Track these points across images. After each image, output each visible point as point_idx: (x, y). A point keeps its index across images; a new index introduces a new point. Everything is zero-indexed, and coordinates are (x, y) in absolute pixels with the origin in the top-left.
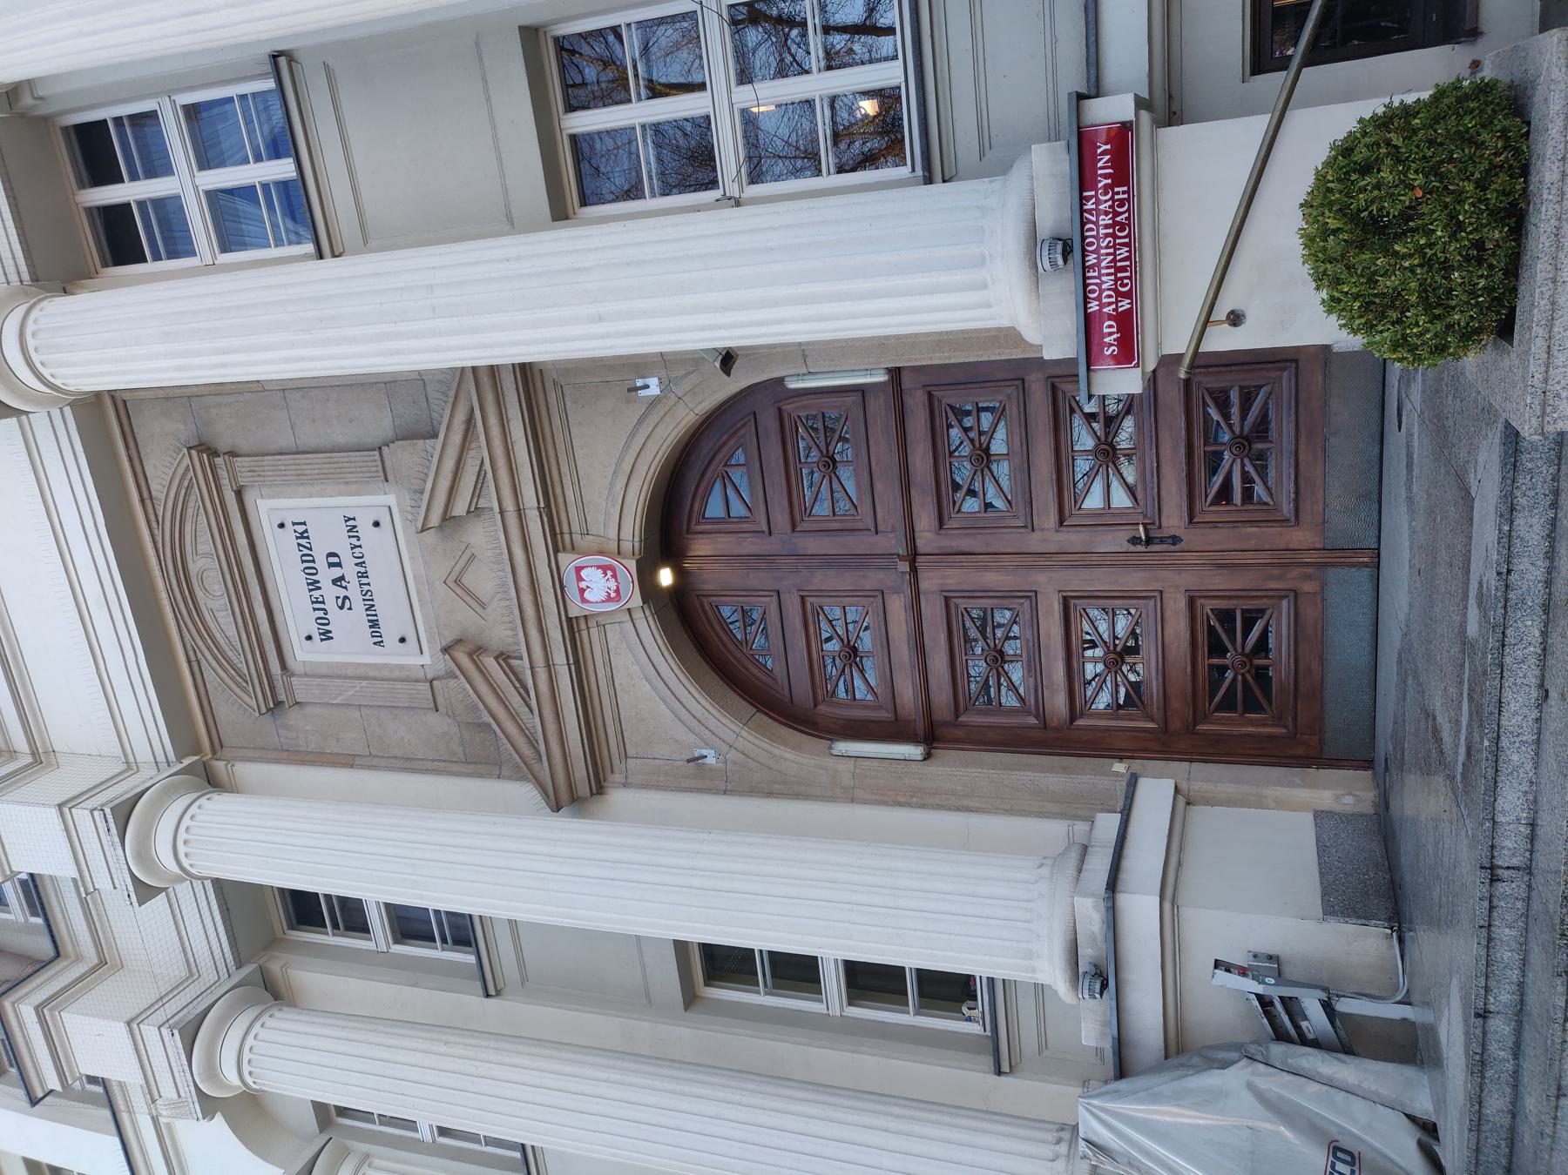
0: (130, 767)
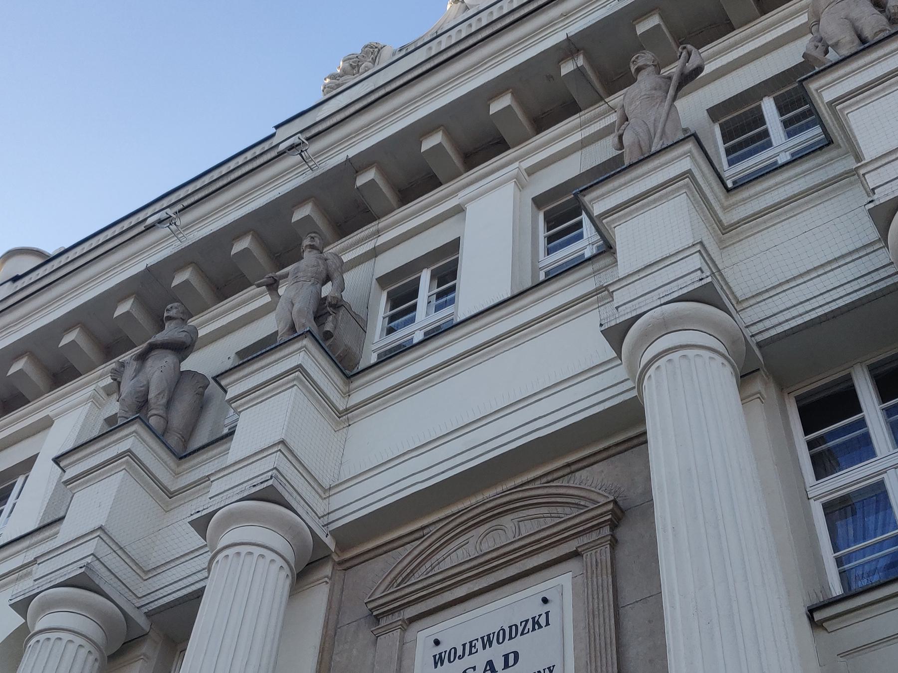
0: (327, 492)
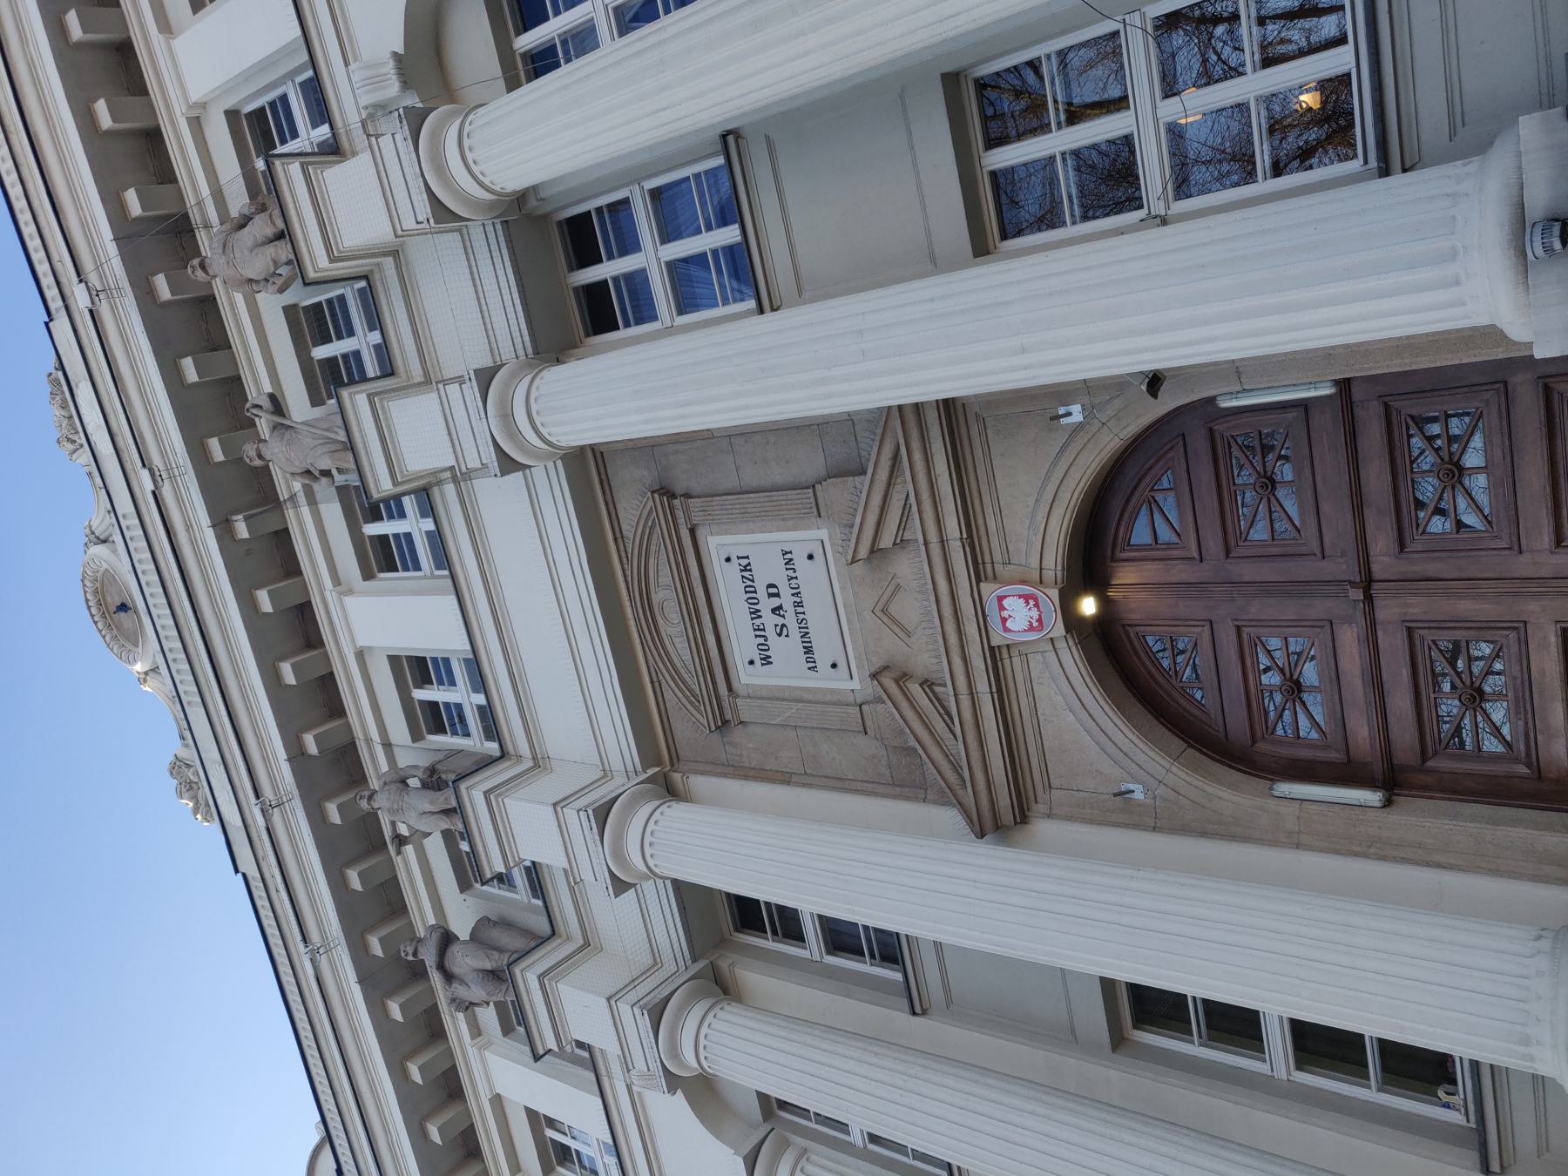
0: (606, 774)
